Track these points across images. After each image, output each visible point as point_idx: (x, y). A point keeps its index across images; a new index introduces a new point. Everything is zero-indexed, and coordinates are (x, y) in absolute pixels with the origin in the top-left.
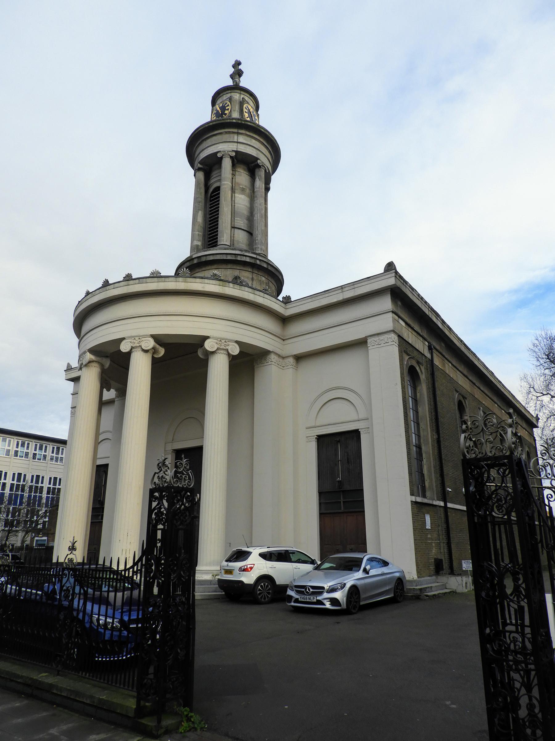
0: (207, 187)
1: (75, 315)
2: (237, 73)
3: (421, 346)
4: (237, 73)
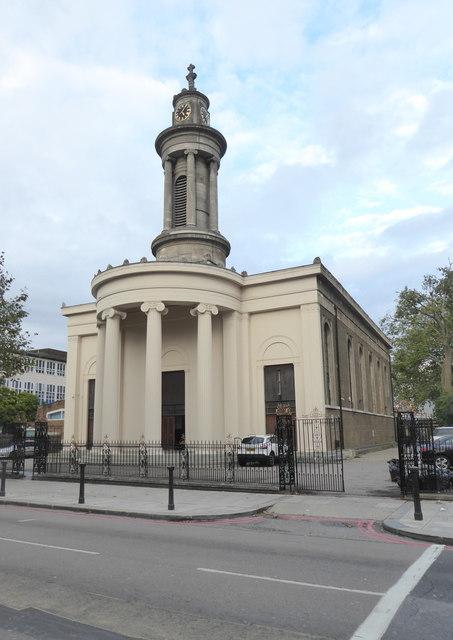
0: (173, 175)
1: (95, 283)
2: (192, 77)
3: (330, 308)
4: (192, 77)
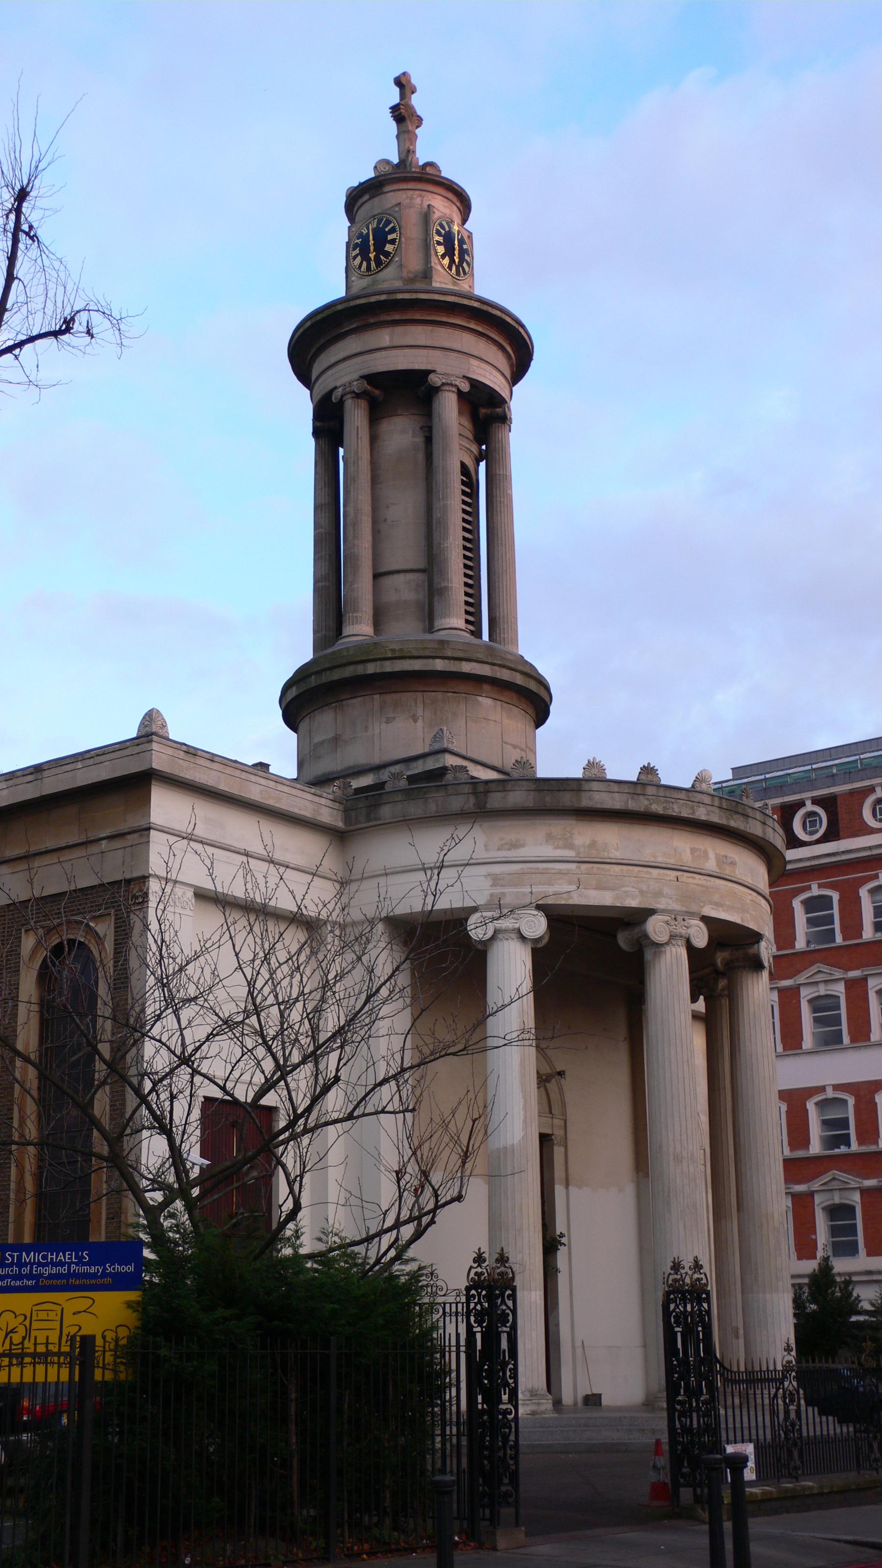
2: (404, 116)
4: (404, 116)
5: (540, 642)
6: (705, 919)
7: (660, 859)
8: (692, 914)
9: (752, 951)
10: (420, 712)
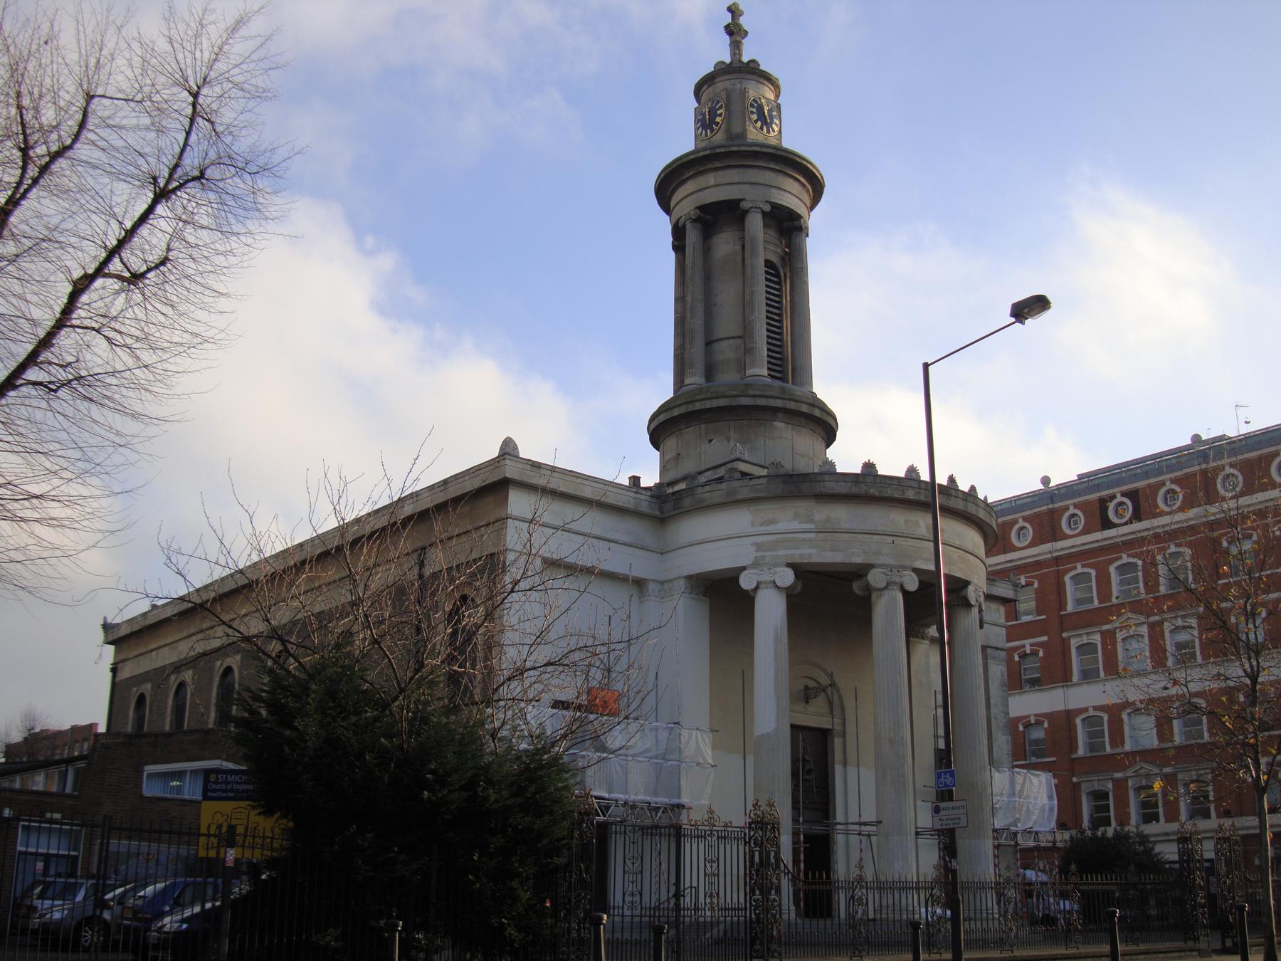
2: (735, 32)
4: (735, 32)
5: (826, 386)
6: (914, 570)
7: (880, 528)
8: (905, 568)
9: (963, 593)
10: (732, 434)
